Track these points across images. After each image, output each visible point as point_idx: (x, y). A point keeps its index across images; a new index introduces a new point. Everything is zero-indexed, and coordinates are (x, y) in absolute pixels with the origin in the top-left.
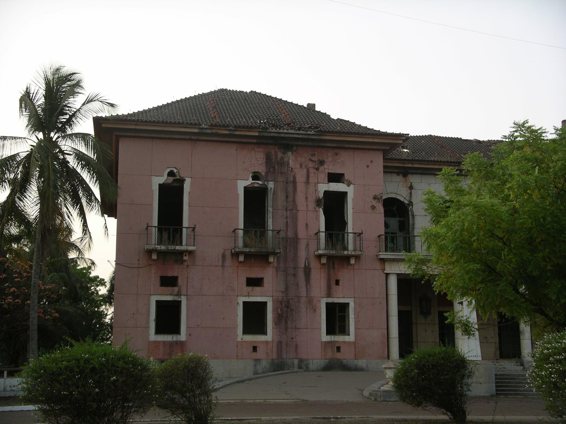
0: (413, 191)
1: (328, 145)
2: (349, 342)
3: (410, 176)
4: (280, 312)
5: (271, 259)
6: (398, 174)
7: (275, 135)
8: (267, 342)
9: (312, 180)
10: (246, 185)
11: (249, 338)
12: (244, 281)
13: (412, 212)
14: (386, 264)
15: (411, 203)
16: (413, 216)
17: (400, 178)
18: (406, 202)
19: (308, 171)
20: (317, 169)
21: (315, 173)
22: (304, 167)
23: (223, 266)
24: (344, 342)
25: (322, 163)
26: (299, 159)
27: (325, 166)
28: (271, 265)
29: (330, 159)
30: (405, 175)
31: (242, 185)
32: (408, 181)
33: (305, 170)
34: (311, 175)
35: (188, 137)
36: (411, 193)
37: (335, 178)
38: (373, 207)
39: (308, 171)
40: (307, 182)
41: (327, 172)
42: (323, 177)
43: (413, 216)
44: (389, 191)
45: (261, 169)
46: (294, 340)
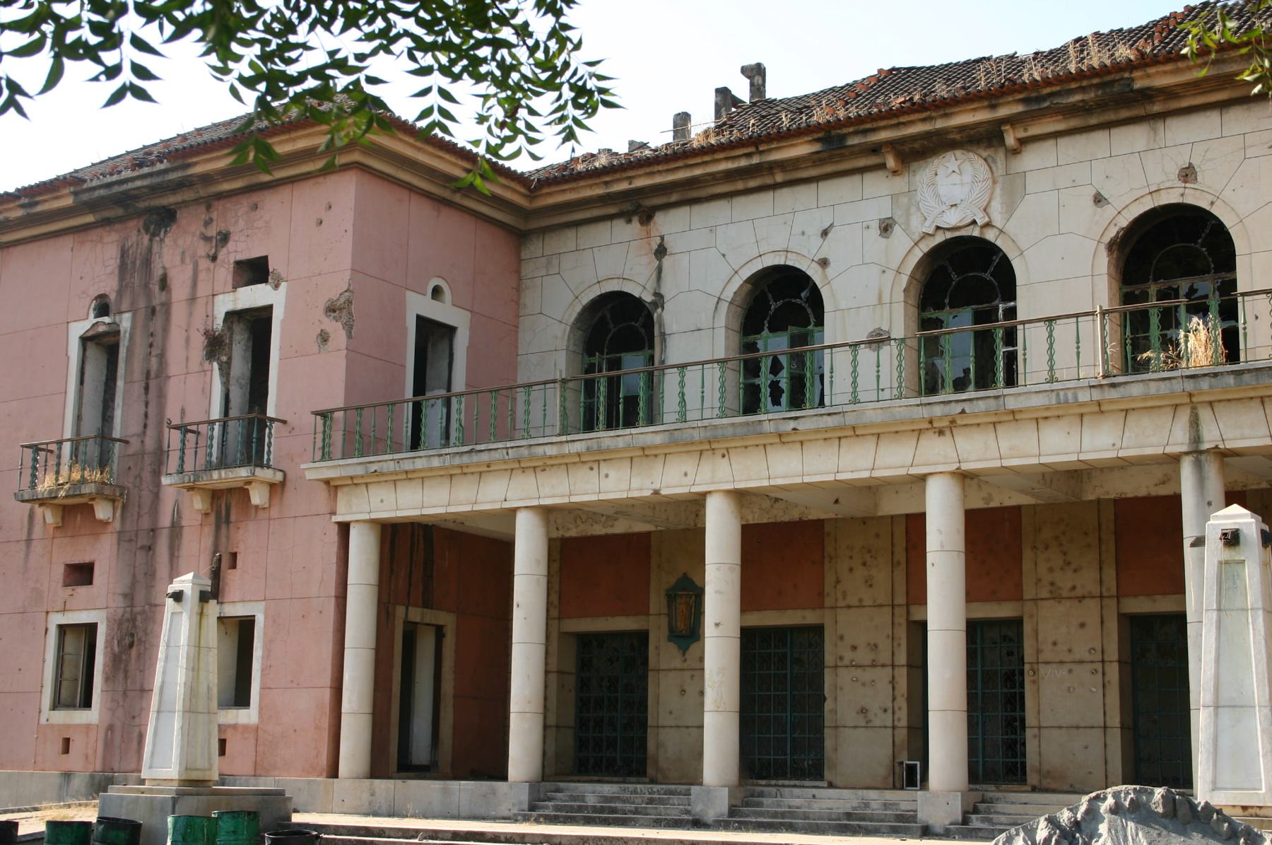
0: (667, 261)
1: (226, 186)
2: (246, 728)
3: (659, 218)
4: (116, 649)
5: (103, 511)
6: (627, 216)
7: (102, 192)
8: (88, 727)
9: (203, 290)
10: (82, 333)
11: (61, 717)
12: (59, 572)
13: (661, 325)
14: (340, 495)
15: (659, 300)
16: (663, 335)
17: (633, 229)
18: (648, 298)
19: (196, 265)
20: (214, 258)
21: (208, 269)
22: (188, 260)
23: (29, 541)
24: (235, 727)
25: (224, 238)
26: (180, 242)
27: (231, 245)
28: (110, 528)
29: (241, 223)
30: (647, 217)
31: (79, 328)
32: (653, 234)
33: (190, 267)
34: (202, 276)
35: (674, 198)
36: (660, 270)
37: (256, 271)
38: (324, 338)
39: (196, 265)
40: (193, 299)
41: (232, 260)
42: (224, 273)
43: (663, 335)
44: (601, 276)
45: (109, 286)
46: (137, 720)
